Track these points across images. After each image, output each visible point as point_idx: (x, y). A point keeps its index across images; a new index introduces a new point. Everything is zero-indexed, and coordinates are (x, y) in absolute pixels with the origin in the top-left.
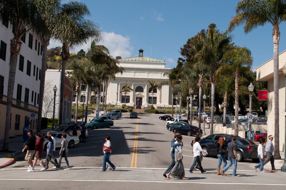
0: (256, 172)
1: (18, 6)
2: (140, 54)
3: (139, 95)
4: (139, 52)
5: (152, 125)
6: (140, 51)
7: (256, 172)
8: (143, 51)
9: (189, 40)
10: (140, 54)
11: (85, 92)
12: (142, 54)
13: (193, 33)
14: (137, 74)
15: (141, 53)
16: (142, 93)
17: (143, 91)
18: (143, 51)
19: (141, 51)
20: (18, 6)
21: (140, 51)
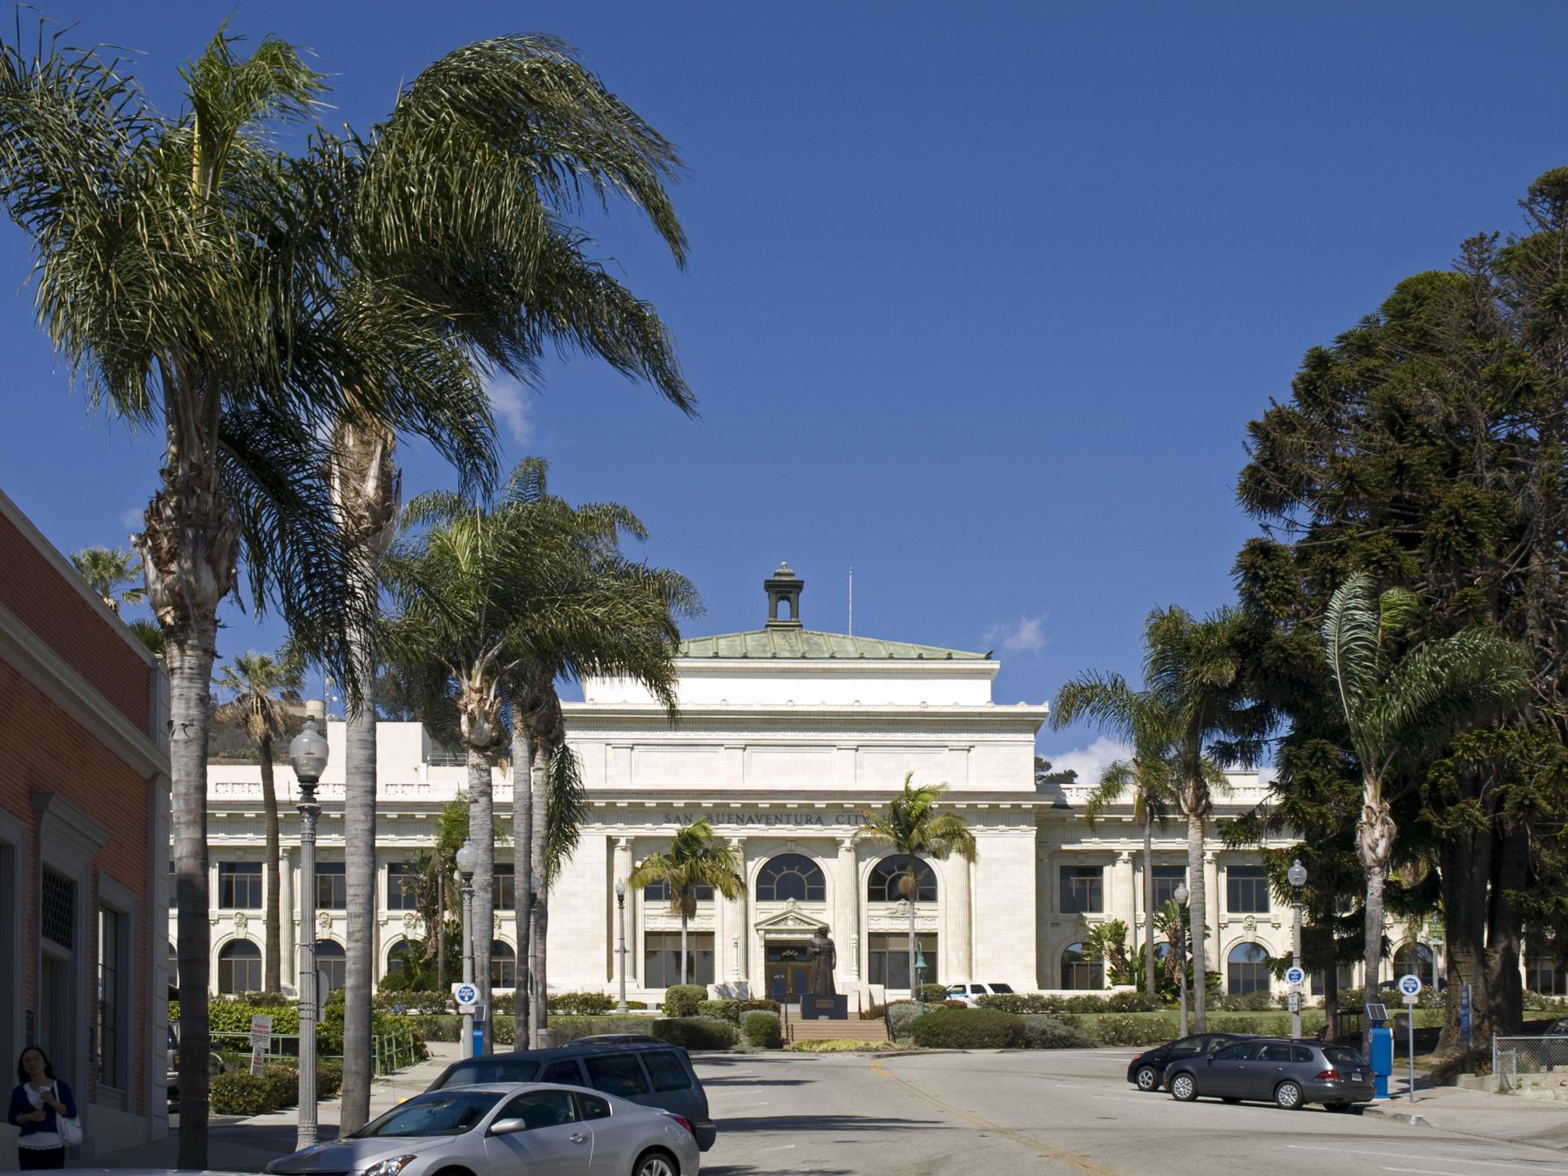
0: (674, 718)
1: (1083, 993)
2: (774, 612)
3: (790, 924)
4: (763, 598)
5: (681, 402)
6: (771, 586)
7: (674, 718)
8: (798, 586)
9: (1319, 361)
10: (774, 612)
11: (248, 912)
12: (795, 612)
13: (1354, 303)
14: (759, 758)
15: (784, 606)
16: (816, 905)
17: (818, 894)
18: (798, 586)
19: (784, 590)
20: (1083, 993)
21: (771, 586)
